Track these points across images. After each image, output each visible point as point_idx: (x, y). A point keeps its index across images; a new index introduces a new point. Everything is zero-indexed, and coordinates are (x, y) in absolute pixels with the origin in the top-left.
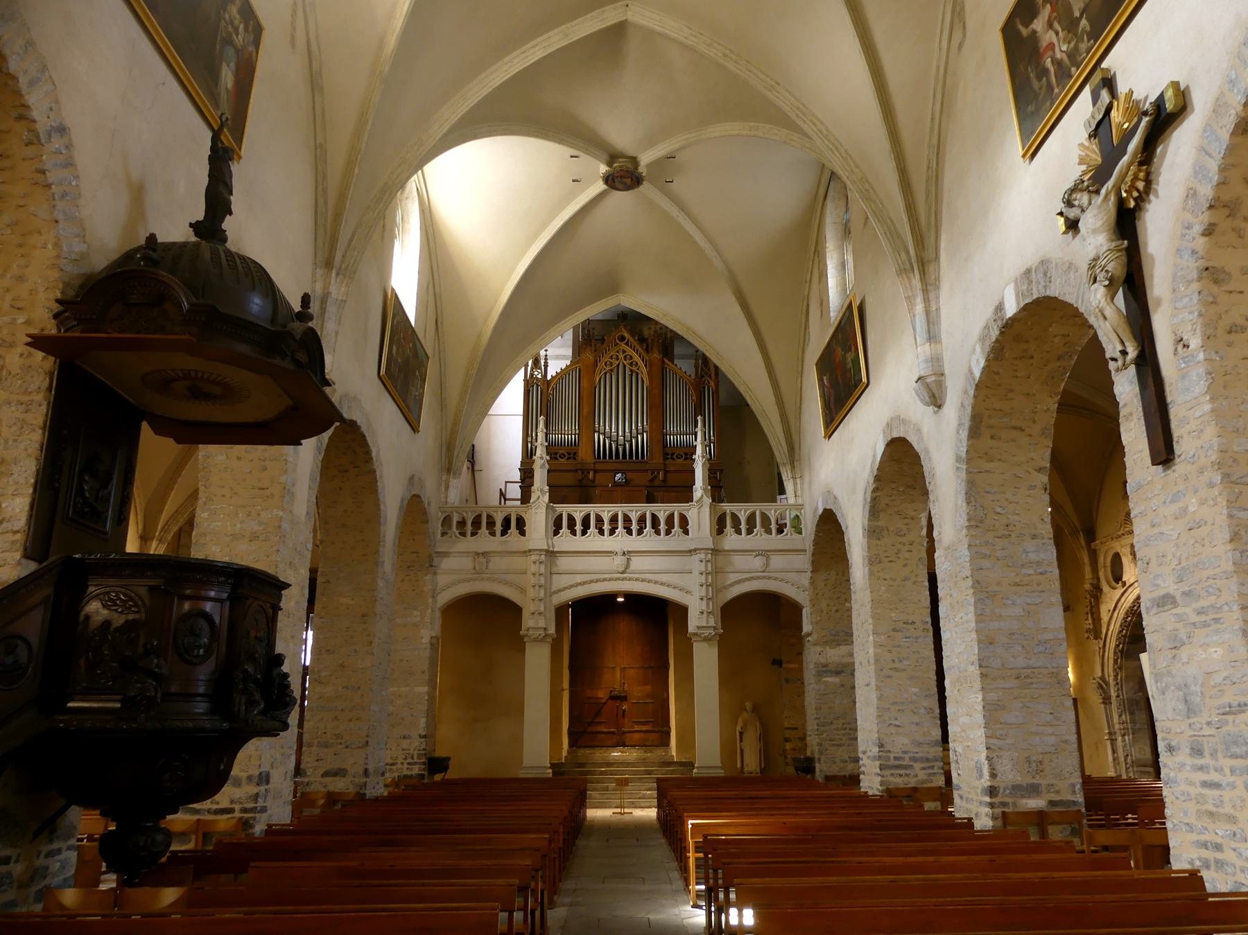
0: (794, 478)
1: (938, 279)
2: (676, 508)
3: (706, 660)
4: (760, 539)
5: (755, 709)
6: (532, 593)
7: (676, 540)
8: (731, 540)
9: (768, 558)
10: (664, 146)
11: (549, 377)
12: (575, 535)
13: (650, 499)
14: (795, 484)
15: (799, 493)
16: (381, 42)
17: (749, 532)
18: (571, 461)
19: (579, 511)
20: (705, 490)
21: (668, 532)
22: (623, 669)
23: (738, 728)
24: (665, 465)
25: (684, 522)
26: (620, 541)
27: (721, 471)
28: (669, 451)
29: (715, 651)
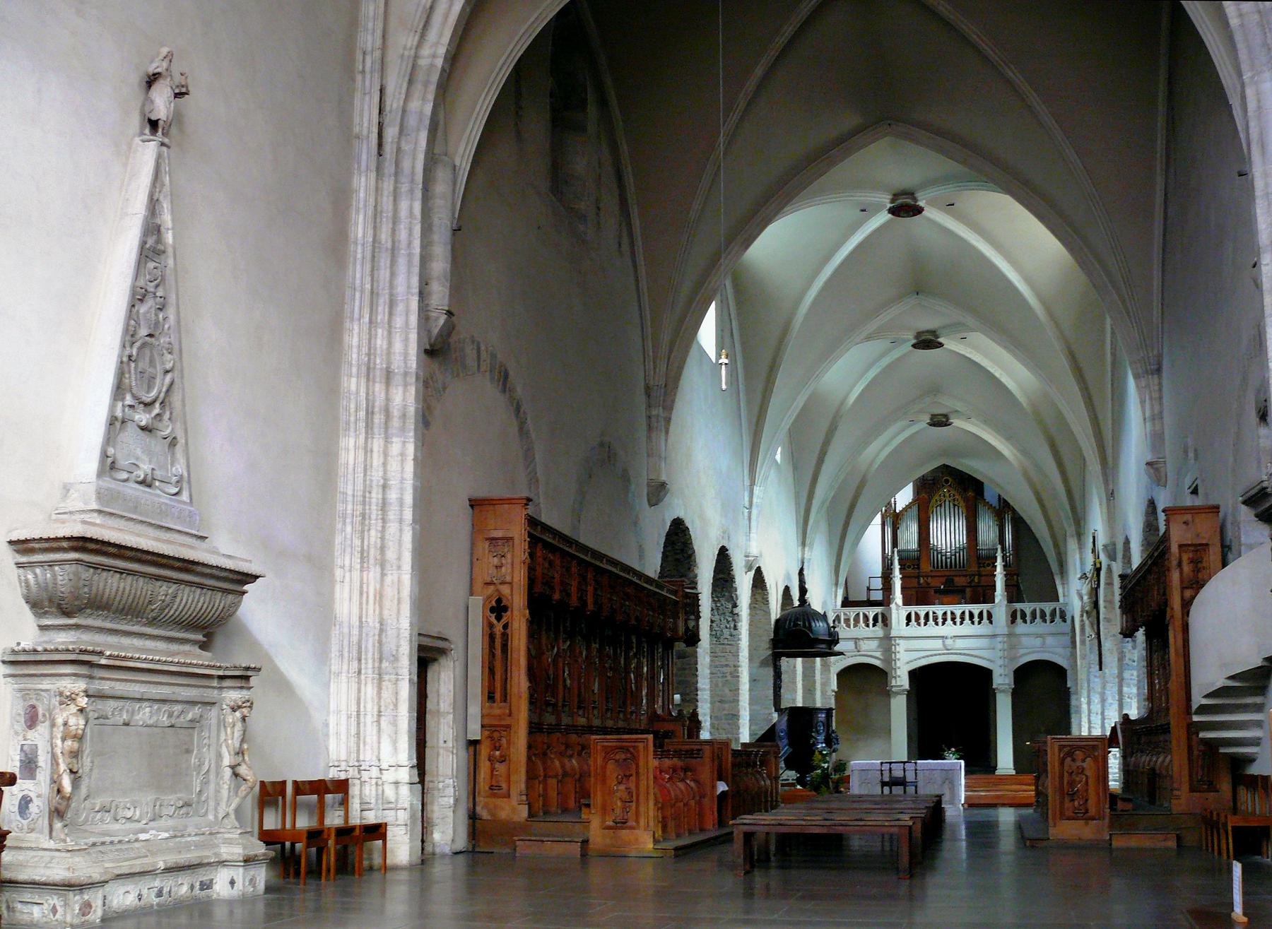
2: (985, 607)
4: (1039, 627)
7: (984, 628)
8: (1021, 627)
9: (1044, 638)
12: (1065, 622)
14: (1064, 588)
19: (922, 610)
21: (1052, 621)
25: (990, 616)
26: (949, 629)
27: (1018, 575)
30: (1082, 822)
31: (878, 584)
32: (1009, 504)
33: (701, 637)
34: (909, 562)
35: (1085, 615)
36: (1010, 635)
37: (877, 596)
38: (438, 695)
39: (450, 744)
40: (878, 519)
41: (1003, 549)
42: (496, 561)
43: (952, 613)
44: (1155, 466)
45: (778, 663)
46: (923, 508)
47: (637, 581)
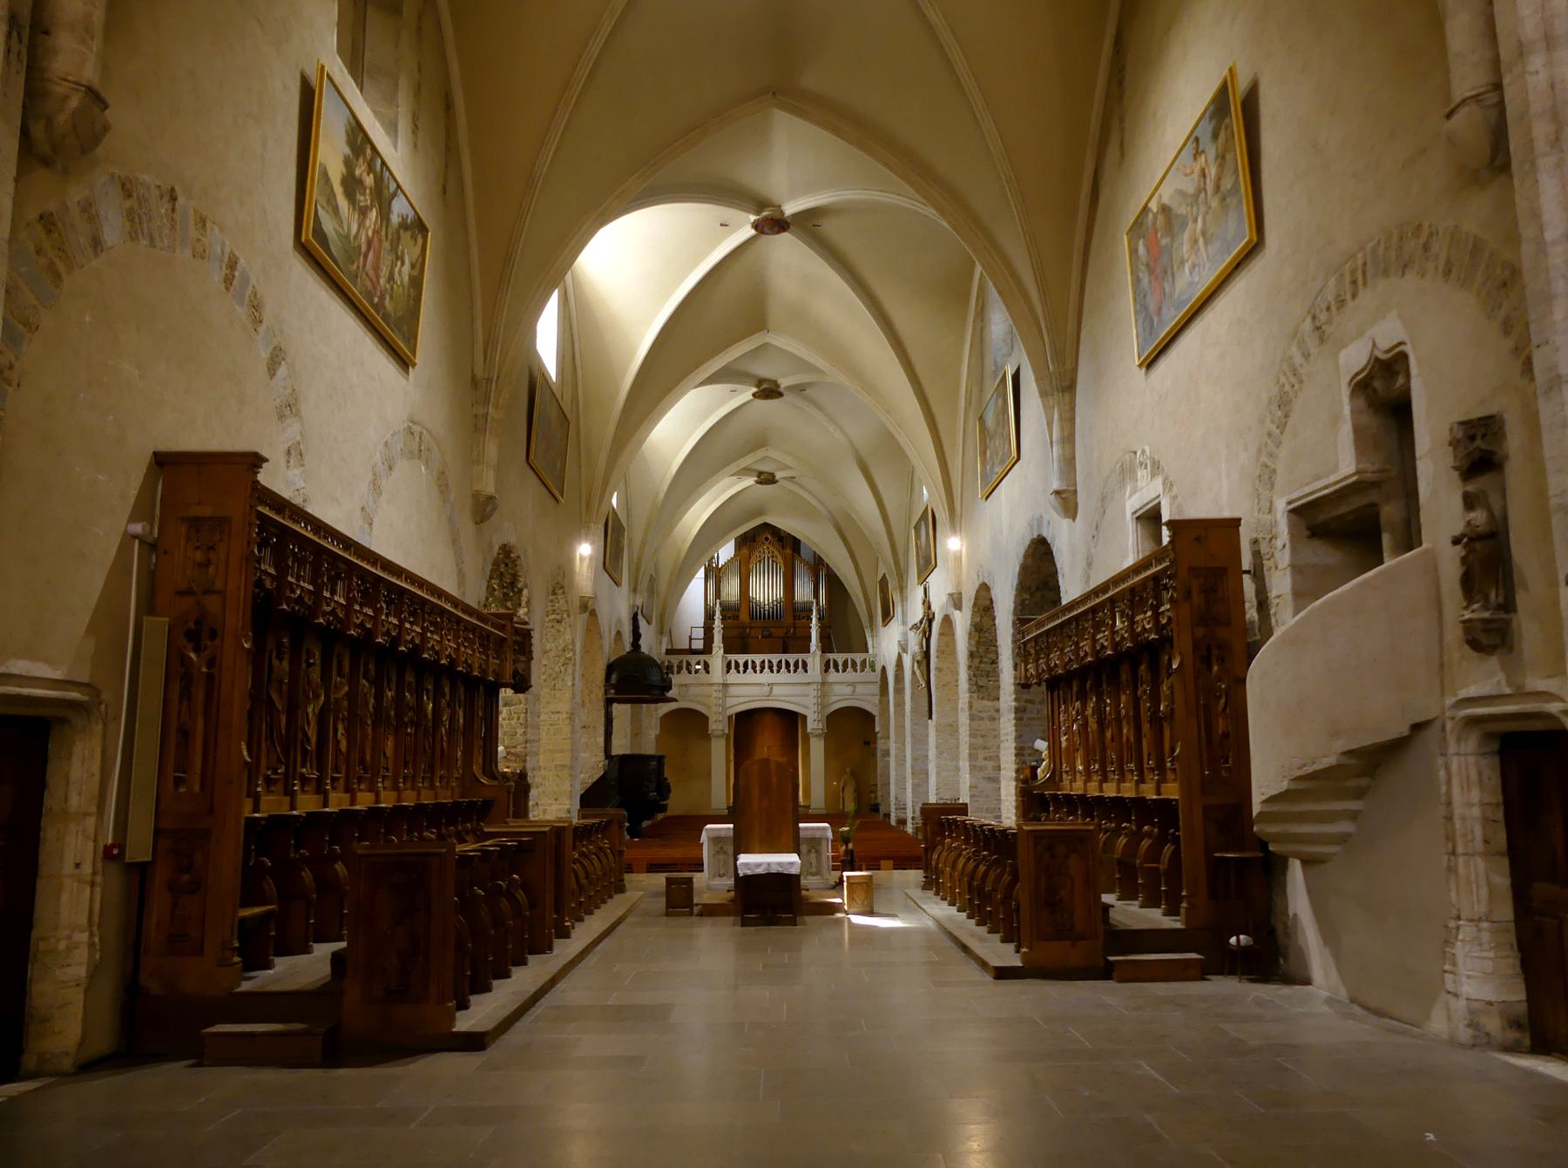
0: (872, 636)
1: (907, 597)
2: (800, 657)
3: (817, 748)
4: (850, 675)
5: (853, 774)
6: (714, 709)
7: (800, 676)
8: (833, 676)
10: (812, 199)
11: (720, 566)
13: (785, 652)
14: (873, 640)
15: (875, 646)
16: (657, 494)
17: (844, 671)
18: (735, 622)
19: (741, 658)
20: (817, 646)
21: (778, 672)
22: (769, 747)
23: (842, 785)
24: (794, 623)
26: (767, 677)
28: (797, 614)
29: (823, 742)
30: (1068, 943)
31: (700, 633)
32: (823, 560)
33: (532, 683)
34: (730, 612)
35: (916, 664)
36: (823, 683)
37: (699, 645)
38: (68, 783)
39: (87, 869)
40: (701, 573)
41: (818, 604)
42: (199, 556)
43: (770, 662)
44: (1064, 496)
45: (609, 709)
46: (744, 568)
47: (452, 610)
